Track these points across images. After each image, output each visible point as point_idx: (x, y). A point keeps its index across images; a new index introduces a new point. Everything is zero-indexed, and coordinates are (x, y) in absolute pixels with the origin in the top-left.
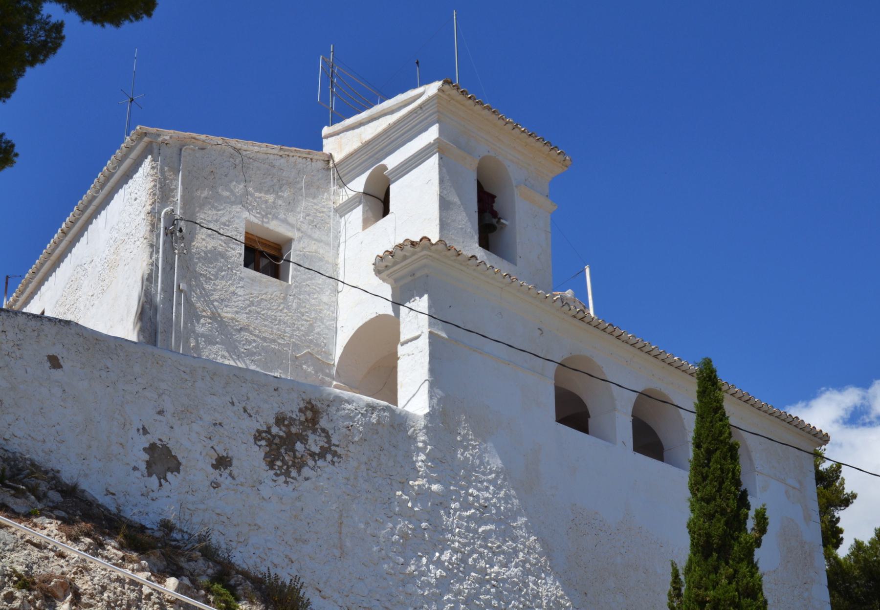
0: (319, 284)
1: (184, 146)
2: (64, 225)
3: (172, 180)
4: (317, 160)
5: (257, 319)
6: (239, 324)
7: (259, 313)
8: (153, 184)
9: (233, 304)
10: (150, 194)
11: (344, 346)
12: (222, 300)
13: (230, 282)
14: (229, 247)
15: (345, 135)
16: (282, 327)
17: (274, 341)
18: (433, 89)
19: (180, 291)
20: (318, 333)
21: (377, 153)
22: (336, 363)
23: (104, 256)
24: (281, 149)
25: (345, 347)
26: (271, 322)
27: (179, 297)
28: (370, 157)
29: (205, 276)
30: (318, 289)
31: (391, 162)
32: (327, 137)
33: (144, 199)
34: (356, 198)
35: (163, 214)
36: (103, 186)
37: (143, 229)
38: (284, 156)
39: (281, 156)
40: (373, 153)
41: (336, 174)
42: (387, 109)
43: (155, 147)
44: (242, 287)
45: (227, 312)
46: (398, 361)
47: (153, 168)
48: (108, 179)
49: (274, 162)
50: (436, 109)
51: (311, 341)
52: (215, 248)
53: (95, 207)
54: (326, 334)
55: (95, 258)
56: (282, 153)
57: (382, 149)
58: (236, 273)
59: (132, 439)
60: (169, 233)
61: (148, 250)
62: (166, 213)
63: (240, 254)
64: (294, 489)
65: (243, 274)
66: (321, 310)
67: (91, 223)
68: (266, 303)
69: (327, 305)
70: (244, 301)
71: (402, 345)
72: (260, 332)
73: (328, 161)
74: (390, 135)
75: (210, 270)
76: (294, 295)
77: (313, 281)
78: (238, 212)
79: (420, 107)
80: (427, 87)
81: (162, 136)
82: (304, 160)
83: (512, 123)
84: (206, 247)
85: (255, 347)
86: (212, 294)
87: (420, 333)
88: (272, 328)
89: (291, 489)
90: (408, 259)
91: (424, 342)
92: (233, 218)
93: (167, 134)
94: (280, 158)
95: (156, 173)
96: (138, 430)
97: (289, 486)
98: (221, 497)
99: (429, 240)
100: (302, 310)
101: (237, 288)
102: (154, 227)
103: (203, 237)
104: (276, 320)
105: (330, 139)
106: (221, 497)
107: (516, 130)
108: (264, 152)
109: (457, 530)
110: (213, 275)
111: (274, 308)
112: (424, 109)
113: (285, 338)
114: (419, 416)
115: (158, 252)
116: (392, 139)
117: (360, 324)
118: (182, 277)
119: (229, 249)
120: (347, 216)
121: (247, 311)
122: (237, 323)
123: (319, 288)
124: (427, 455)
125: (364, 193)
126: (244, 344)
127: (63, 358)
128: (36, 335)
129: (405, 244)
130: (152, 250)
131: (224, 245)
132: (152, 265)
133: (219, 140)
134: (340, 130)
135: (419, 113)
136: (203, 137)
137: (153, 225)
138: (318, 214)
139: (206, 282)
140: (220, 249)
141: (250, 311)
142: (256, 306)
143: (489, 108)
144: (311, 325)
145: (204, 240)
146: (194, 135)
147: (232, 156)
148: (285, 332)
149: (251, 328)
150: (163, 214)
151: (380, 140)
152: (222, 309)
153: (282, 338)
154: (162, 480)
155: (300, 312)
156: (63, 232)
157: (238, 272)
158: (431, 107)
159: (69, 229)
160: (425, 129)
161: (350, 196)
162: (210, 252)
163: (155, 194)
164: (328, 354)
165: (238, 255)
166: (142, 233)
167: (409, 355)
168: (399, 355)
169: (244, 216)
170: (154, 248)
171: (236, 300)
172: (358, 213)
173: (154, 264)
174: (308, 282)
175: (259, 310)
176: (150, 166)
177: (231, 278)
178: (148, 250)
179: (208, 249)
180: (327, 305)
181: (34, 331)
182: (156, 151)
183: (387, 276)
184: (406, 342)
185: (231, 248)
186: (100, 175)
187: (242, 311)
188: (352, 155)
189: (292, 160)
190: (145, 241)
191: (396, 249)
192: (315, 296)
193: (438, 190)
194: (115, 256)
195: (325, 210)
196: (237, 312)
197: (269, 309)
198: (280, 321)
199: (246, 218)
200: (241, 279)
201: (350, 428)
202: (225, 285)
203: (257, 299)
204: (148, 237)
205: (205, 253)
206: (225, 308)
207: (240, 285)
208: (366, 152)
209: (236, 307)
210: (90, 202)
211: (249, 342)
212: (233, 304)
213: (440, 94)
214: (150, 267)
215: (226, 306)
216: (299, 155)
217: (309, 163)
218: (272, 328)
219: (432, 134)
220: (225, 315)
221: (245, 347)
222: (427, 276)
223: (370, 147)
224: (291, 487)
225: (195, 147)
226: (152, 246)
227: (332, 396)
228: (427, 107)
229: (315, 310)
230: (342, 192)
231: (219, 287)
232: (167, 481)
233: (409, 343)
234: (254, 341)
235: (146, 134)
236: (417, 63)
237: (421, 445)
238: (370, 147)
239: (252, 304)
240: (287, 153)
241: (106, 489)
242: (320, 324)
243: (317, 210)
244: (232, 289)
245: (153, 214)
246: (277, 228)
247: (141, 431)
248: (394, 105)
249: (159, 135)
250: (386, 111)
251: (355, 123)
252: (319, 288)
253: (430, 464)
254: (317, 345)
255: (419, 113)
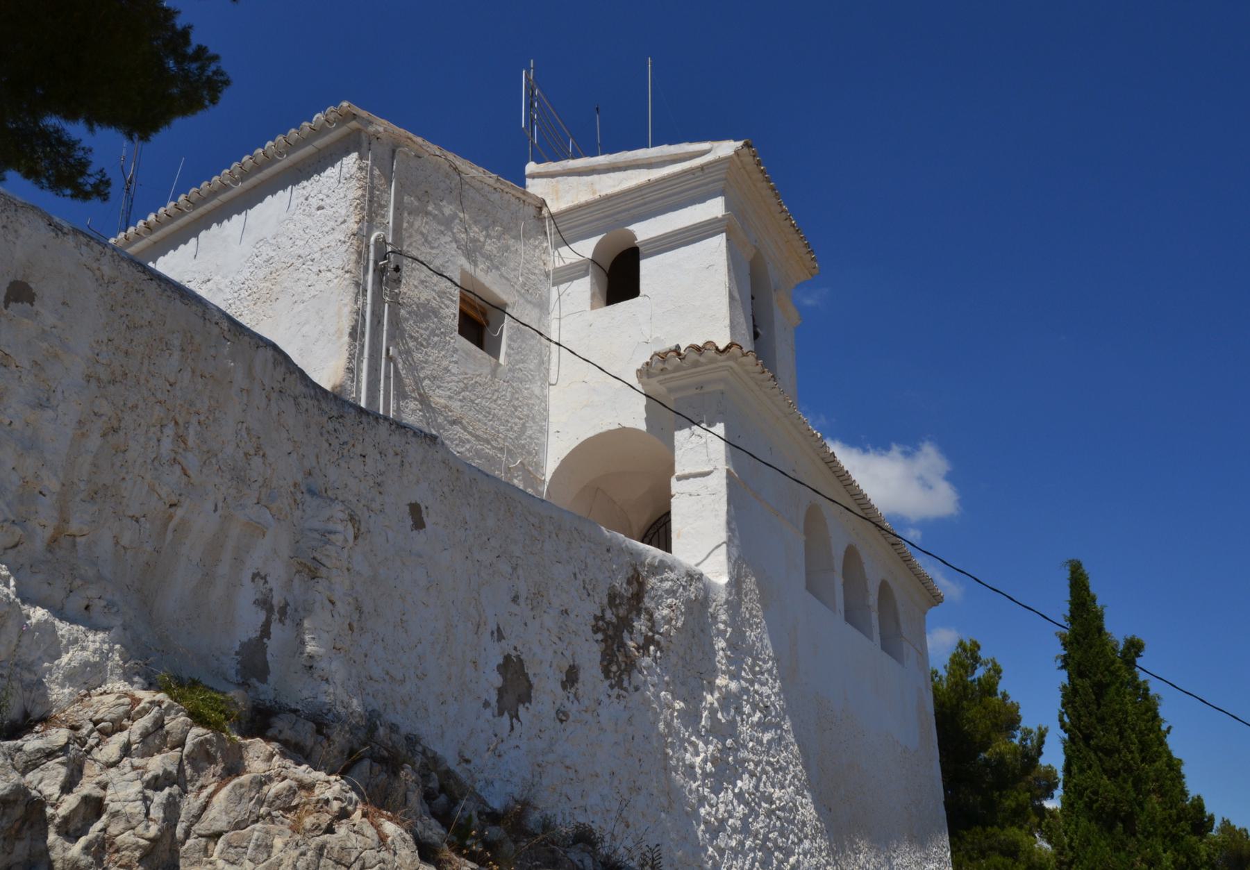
0: (532, 371)
1: (398, 147)
2: (151, 217)
3: (382, 192)
4: (529, 204)
5: (470, 410)
6: (453, 416)
7: (473, 402)
8: (360, 192)
9: (446, 384)
10: (356, 207)
11: (561, 459)
12: (435, 378)
13: (443, 353)
14: (443, 303)
15: (558, 182)
16: (496, 424)
17: (488, 442)
18: (726, 148)
19: (390, 358)
20: (530, 437)
21: (619, 213)
22: (548, 479)
23: (241, 278)
24: (498, 179)
25: (562, 461)
26: (485, 416)
27: (387, 366)
28: (608, 216)
29: (416, 339)
30: (530, 377)
31: (643, 231)
32: (533, 176)
33: (343, 212)
34: (582, 265)
35: (372, 239)
36: (245, 175)
37: (343, 256)
38: (498, 190)
39: (495, 189)
40: (612, 212)
41: (553, 226)
42: (644, 159)
43: (364, 138)
44: (456, 362)
45: (439, 396)
46: (672, 500)
47: (360, 169)
48: (258, 168)
49: (489, 195)
50: (724, 176)
51: (523, 446)
52: (429, 301)
53: (221, 203)
54: (538, 439)
55: (217, 278)
56: (498, 185)
57: (628, 210)
58: (449, 341)
59: (485, 650)
60: (380, 272)
61: (352, 290)
62: (376, 240)
63: (455, 315)
64: (625, 707)
65: (457, 343)
66: (533, 405)
67: (208, 227)
68: (480, 388)
69: (539, 399)
70: (458, 382)
71: (679, 479)
72: (474, 429)
73: (541, 209)
74: (645, 194)
75: (422, 332)
76: (508, 382)
77: (526, 365)
78: (453, 256)
79: (702, 168)
80: (716, 144)
81: (374, 125)
82: (517, 200)
83: (786, 212)
84: (419, 298)
85: (468, 450)
86: (423, 368)
87: (712, 469)
88: (485, 424)
89: (622, 707)
90: (700, 366)
91: (719, 482)
92: (447, 262)
93: (381, 126)
94: (493, 191)
95: (365, 178)
96: (492, 633)
97: (621, 702)
98: (568, 737)
99: (741, 348)
100: (516, 403)
101: (450, 362)
102: (361, 255)
103: (416, 283)
104: (490, 414)
105: (537, 181)
106: (568, 737)
107: (788, 221)
108: (480, 179)
109: (751, 744)
110: (425, 339)
111: (489, 396)
112: (706, 171)
113: (499, 439)
114: (720, 586)
115: (365, 295)
116: (647, 200)
117: (591, 434)
118: (391, 338)
119: (443, 306)
120: (563, 287)
121: (461, 397)
122: (450, 414)
123: (531, 375)
124: (727, 641)
125: (592, 260)
126: (457, 445)
127: (427, 508)
128: (399, 463)
129: (708, 347)
130: (356, 291)
131: (438, 299)
132: (358, 315)
133: (435, 149)
134: (557, 171)
135: (696, 175)
136: (419, 140)
137: (360, 254)
138: (530, 276)
139: (417, 349)
140: (434, 304)
141: (464, 398)
142: (470, 392)
143: (773, 189)
144: (524, 425)
145: (416, 287)
146: (410, 135)
147: (447, 175)
148: (498, 432)
149: (464, 421)
150: (372, 239)
151: (628, 198)
152: (434, 391)
153: (496, 440)
154: (514, 720)
155: (513, 406)
156: (147, 225)
157: (452, 341)
158: (717, 171)
159: (160, 224)
160: (701, 199)
161: (568, 262)
162: (424, 306)
163: (362, 208)
164: (539, 466)
165: (452, 316)
166: (339, 263)
167: (690, 495)
168: (673, 491)
169: (460, 263)
170: (359, 286)
171: (449, 379)
172: (583, 288)
173: (360, 313)
174: (521, 366)
175: (473, 397)
176: (356, 166)
177: (444, 346)
178: (352, 290)
179: (421, 301)
180: (539, 399)
181: (397, 454)
182: (365, 144)
183: (658, 382)
184: (686, 477)
185: (445, 305)
186: (246, 158)
187: (455, 397)
188: (580, 207)
189: (506, 197)
190: (347, 275)
191: (690, 351)
192: (527, 386)
193: (727, 280)
194: (268, 284)
195: (537, 271)
196: (450, 398)
197: (483, 397)
198: (494, 415)
199: (462, 265)
200: (455, 351)
201: (674, 608)
202: (438, 357)
203: (471, 382)
204: (354, 270)
205: (417, 307)
206: (437, 390)
207: (454, 359)
208: (603, 209)
209: (450, 389)
210: (213, 194)
211: (463, 442)
212: (446, 384)
213: (736, 158)
214: (355, 317)
215: (439, 387)
216: (513, 192)
217: (521, 206)
218: (485, 424)
219: (715, 208)
220: (437, 399)
221: (458, 449)
222: (723, 393)
223: (609, 204)
224: (623, 703)
225: (411, 150)
226: (357, 284)
227: (657, 560)
228: (711, 170)
229: (527, 405)
230: (564, 250)
231: (431, 359)
232: (519, 721)
233: (691, 479)
234: (469, 441)
235: (355, 116)
236: (597, 109)
237: (722, 626)
238: (609, 204)
239: (465, 388)
240: (502, 187)
241: (459, 753)
242: (532, 424)
243: (529, 270)
244: (445, 363)
245: (360, 236)
246: (493, 284)
247: (496, 634)
248: (657, 157)
249: (371, 123)
250: (640, 162)
251: (587, 167)
252: (531, 375)
253: (729, 653)
254: (529, 453)
255: (696, 175)
